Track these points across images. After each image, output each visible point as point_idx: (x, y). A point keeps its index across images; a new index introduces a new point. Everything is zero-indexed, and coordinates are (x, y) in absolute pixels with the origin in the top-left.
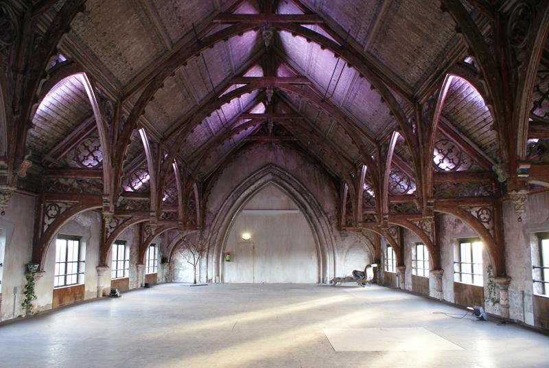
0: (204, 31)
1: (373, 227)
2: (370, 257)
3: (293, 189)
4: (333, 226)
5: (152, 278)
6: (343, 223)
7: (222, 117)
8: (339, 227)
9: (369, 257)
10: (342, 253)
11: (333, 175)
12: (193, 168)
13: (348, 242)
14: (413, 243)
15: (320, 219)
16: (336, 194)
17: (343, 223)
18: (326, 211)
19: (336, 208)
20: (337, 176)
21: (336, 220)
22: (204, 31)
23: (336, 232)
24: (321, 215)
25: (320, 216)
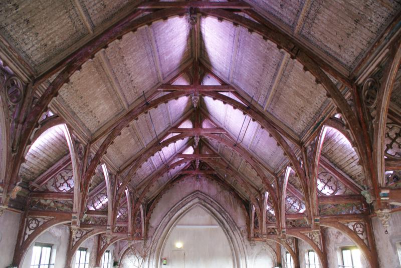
6: (252, 235)
14: (306, 250)
16: (246, 213)
17: (252, 235)
19: (247, 224)
20: (246, 200)
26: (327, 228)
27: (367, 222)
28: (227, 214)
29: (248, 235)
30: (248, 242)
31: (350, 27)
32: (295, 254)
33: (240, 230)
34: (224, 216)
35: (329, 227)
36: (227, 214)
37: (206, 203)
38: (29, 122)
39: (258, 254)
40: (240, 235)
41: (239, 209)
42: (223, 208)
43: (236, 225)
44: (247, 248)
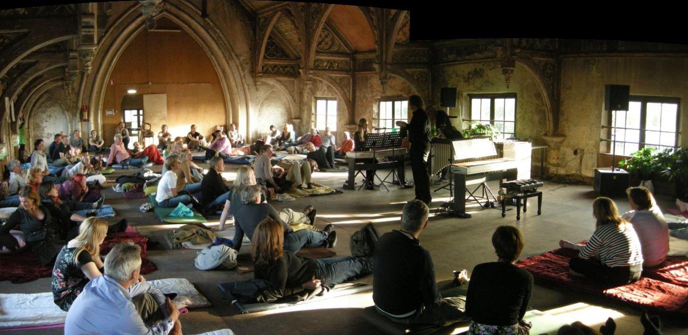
0: (250, 272)
1: (325, 77)
2: (288, 111)
3: (195, 23)
4: (246, 71)
5: (154, 268)
6: (260, 68)
7: (266, 175)
8: (253, 73)
9: (287, 111)
10: (257, 105)
11: (247, 8)
12: (132, 162)
13: (262, 93)
14: (465, 94)
15: (229, 62)
16: (251, 32)
17: (260, 68)
18: (238, 51)
19: (250, 49)
20: (252, 10)
21: (249, 64)
22: (250, 272)
23: (249, 80)
24: (231, 57)
25: (229, 60)
26: (108, 157)
27: (353, 61)
28: (218, 31)
29: (252, 68)
30: (251, 79)
31: (309, 13)
32: (350, 101)
33: (239, 59)
34: (212, 34)
35: (109, 158)
36: (218, 31)
37: (180, 12)
38: (522, 205)
39: (266, 99)
40: (240, 68)
41: (238, 26)
42: (212, 21)
43: (233, 50)
44: (249, 89)
